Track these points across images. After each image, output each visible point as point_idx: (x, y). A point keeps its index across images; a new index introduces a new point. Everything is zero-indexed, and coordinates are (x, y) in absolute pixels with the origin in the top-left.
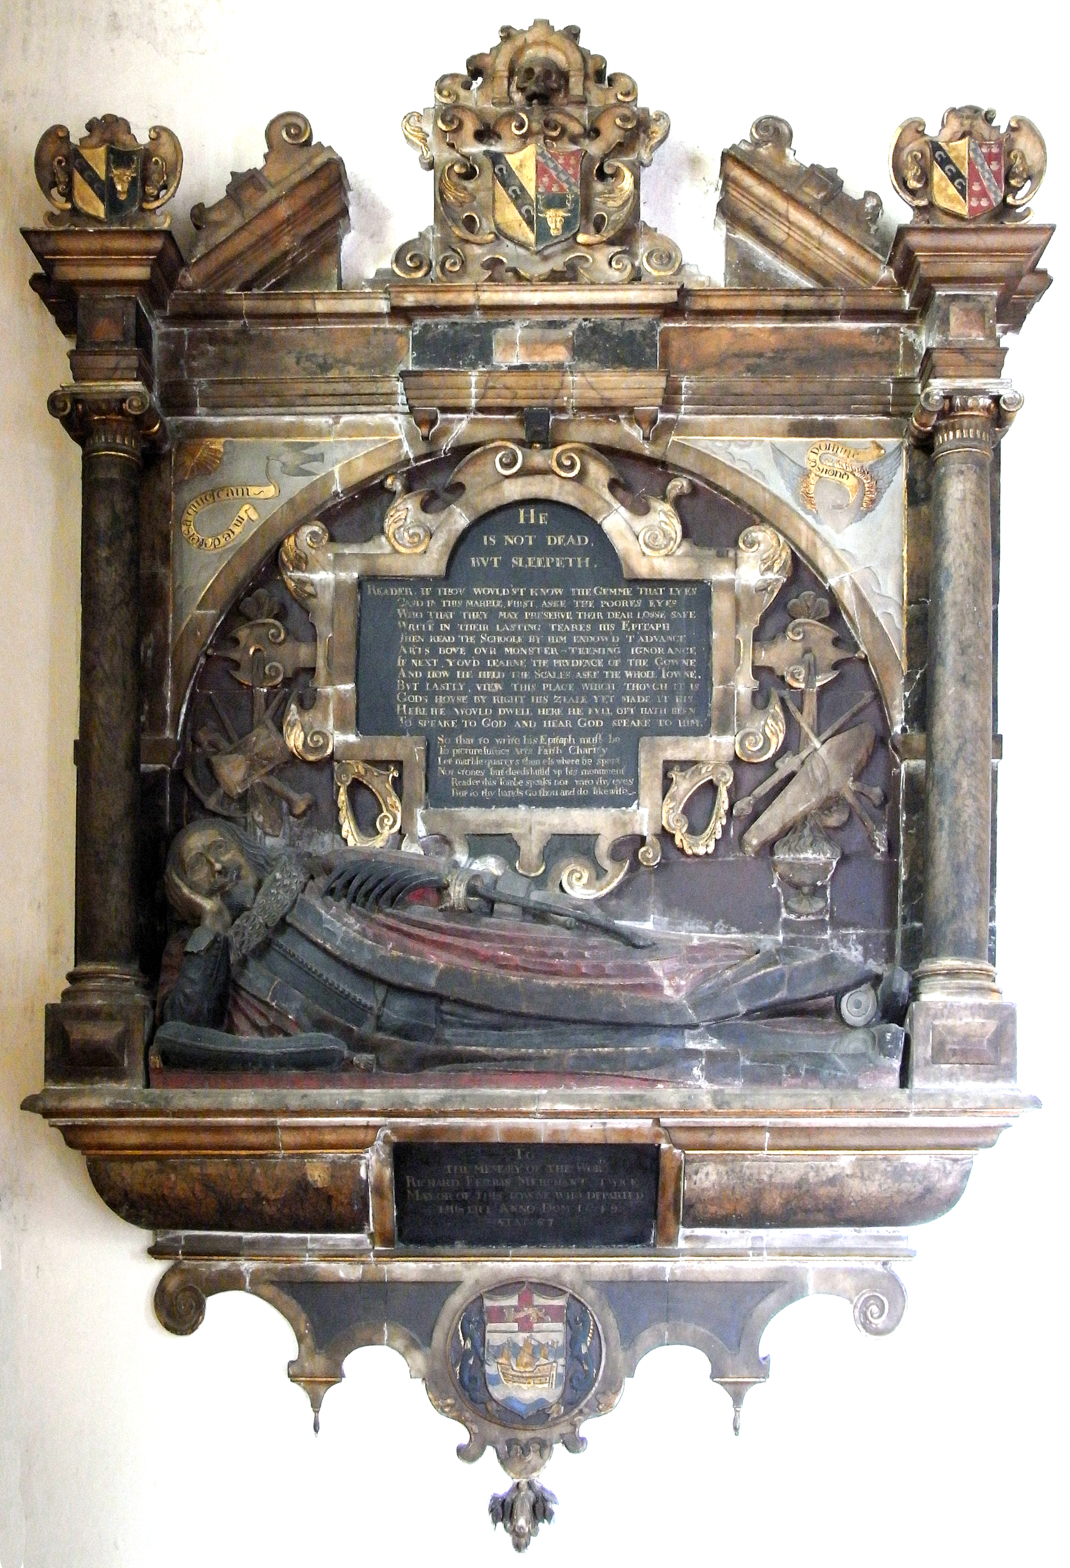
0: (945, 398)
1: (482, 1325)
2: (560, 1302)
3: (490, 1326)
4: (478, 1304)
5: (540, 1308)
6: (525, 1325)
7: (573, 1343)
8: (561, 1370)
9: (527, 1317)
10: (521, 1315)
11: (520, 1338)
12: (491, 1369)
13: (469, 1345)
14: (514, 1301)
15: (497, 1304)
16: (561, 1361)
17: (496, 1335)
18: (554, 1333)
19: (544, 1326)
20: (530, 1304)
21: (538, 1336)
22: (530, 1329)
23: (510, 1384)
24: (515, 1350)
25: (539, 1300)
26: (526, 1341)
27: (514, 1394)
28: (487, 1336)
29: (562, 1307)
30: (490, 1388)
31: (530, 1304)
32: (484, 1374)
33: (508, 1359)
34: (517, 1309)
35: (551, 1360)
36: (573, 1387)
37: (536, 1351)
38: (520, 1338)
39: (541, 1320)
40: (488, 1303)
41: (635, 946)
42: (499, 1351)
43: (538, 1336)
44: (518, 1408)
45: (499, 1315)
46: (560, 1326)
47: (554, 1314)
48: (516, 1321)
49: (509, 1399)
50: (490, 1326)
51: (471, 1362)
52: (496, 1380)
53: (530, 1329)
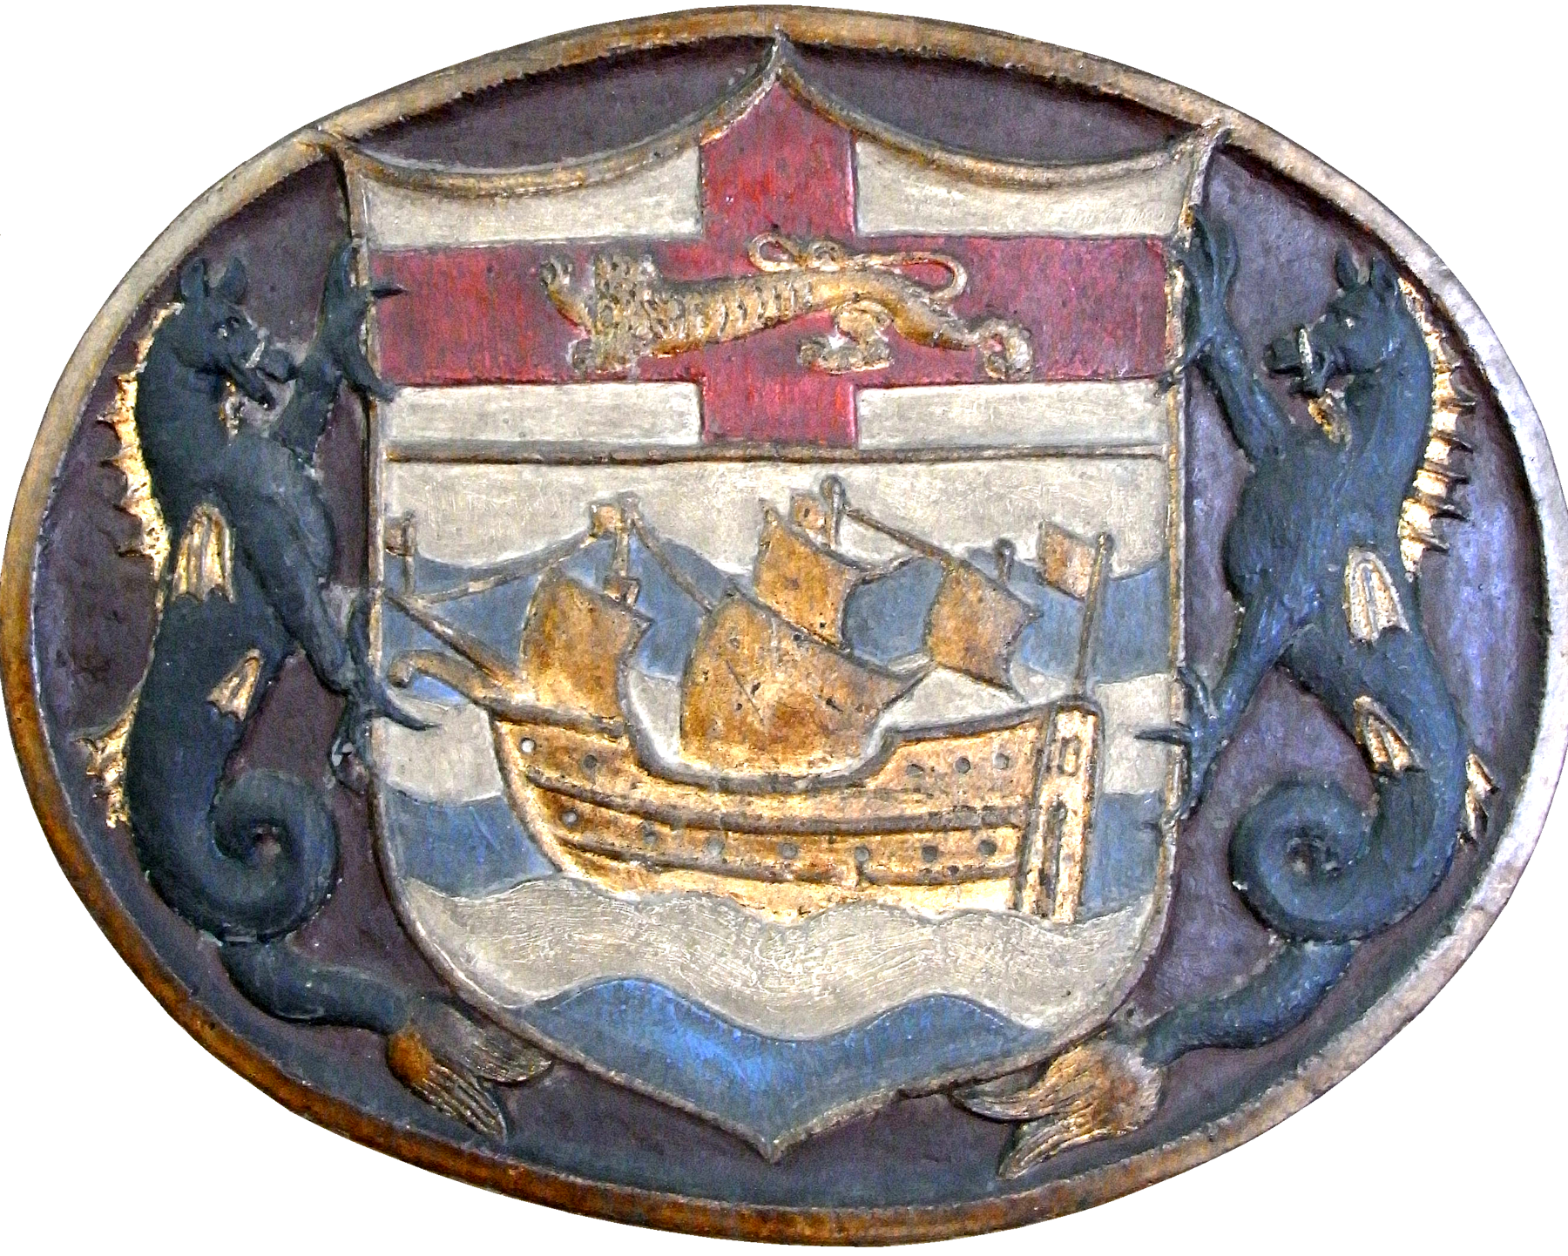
0: (424, 323)
1: (342, 397)
2: (1129, 206)
3: (413, 413)
4: (298, 225)
5: (922, 257)
6: (774, 401)
7: (1251, 548)
8: (1133, 770)
9: (789, 340)
10: (732, 314)
11: (723, 509)
12: (432, 758)
13: (210, 560)
14: (659, 200)
15: (485, 229)
16: (1144, 698)
17: (472, 482)
18: (1086, 467)
19: (963, 407)
20: (826, 226)
21: (906, 494)
22: (821, 433)
23: (620, 887)
24: (668, 601)
25: (899, 195)
26: (777, 533)
27: (665, 959)
28: (395, 490)
29: (1144, 251)
30: (426, 911)
31: (826, 226)
32: (362, 793)
33: (603, 678)
34: (682, 271)
35: (1045, 685)
36: (1254, 909)
37: (879, 614)
38: (723, 509)
39: (925, 357)
40: (397, 222)
41: (230, 757)
42: (496, 625)
43: (906, 494)
44: (700, 1072)
45: (513, 319)
46: (1129, 408)
47: (1087, 312)
48: (676, 365)
49: (623, 997)
50: (413, 413)
51: (235, 695)
52: (483, 847)
53: (821, 433)
